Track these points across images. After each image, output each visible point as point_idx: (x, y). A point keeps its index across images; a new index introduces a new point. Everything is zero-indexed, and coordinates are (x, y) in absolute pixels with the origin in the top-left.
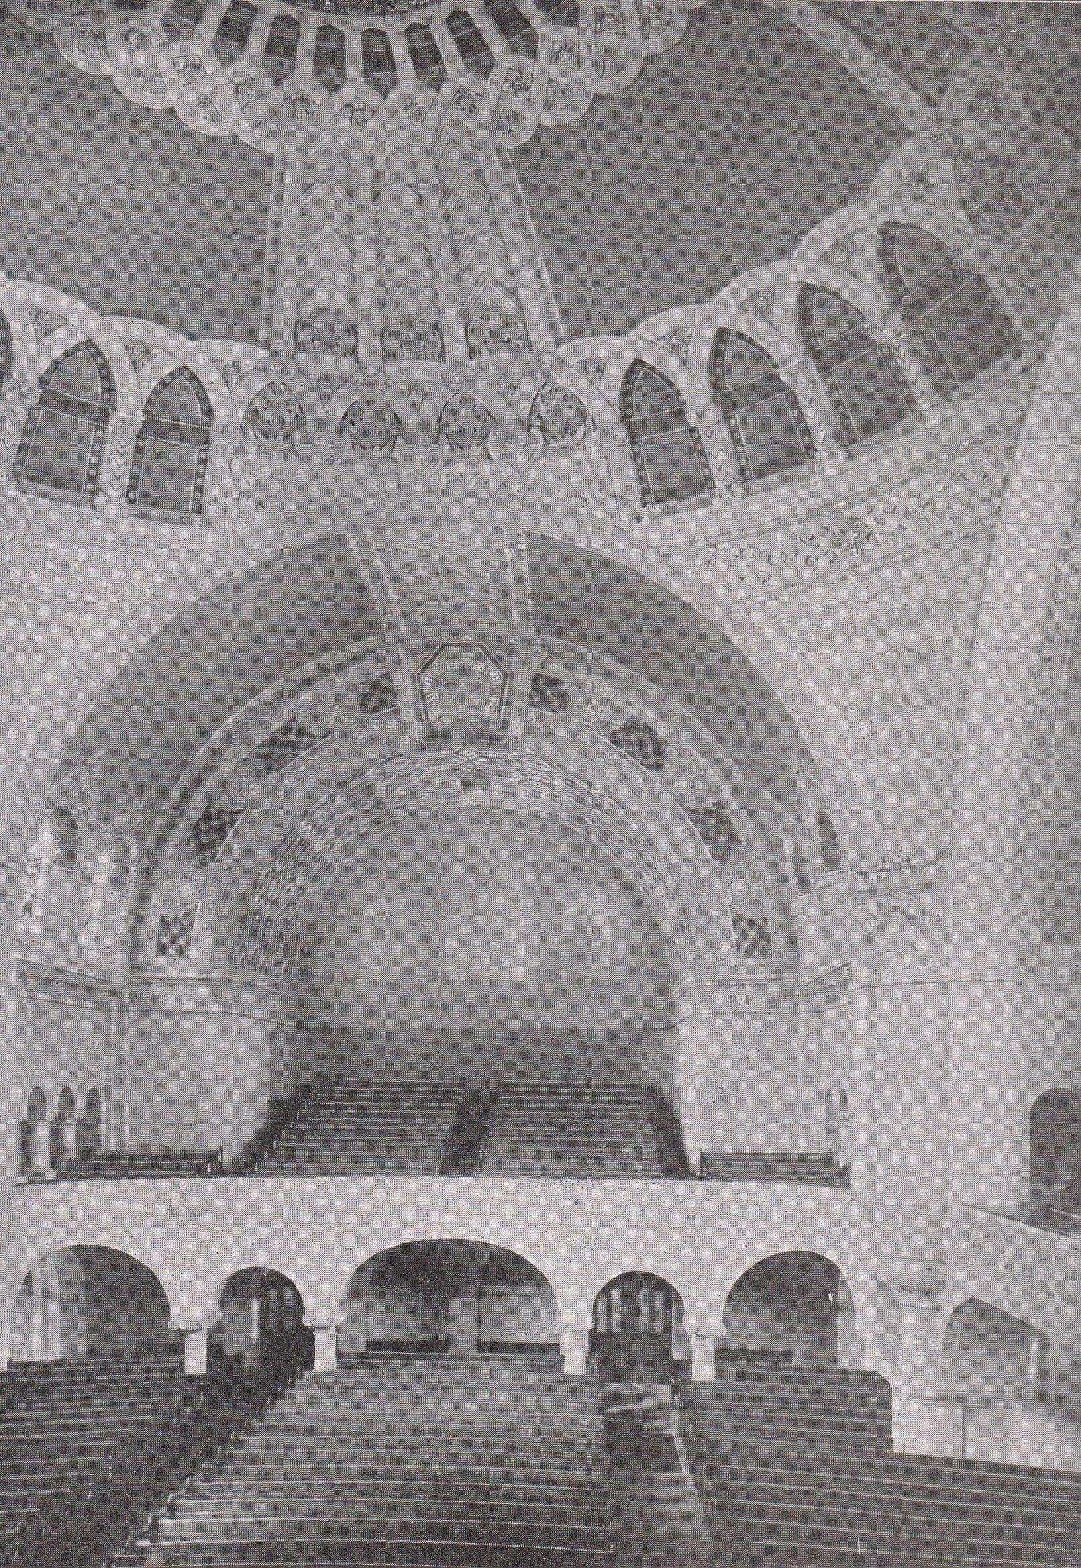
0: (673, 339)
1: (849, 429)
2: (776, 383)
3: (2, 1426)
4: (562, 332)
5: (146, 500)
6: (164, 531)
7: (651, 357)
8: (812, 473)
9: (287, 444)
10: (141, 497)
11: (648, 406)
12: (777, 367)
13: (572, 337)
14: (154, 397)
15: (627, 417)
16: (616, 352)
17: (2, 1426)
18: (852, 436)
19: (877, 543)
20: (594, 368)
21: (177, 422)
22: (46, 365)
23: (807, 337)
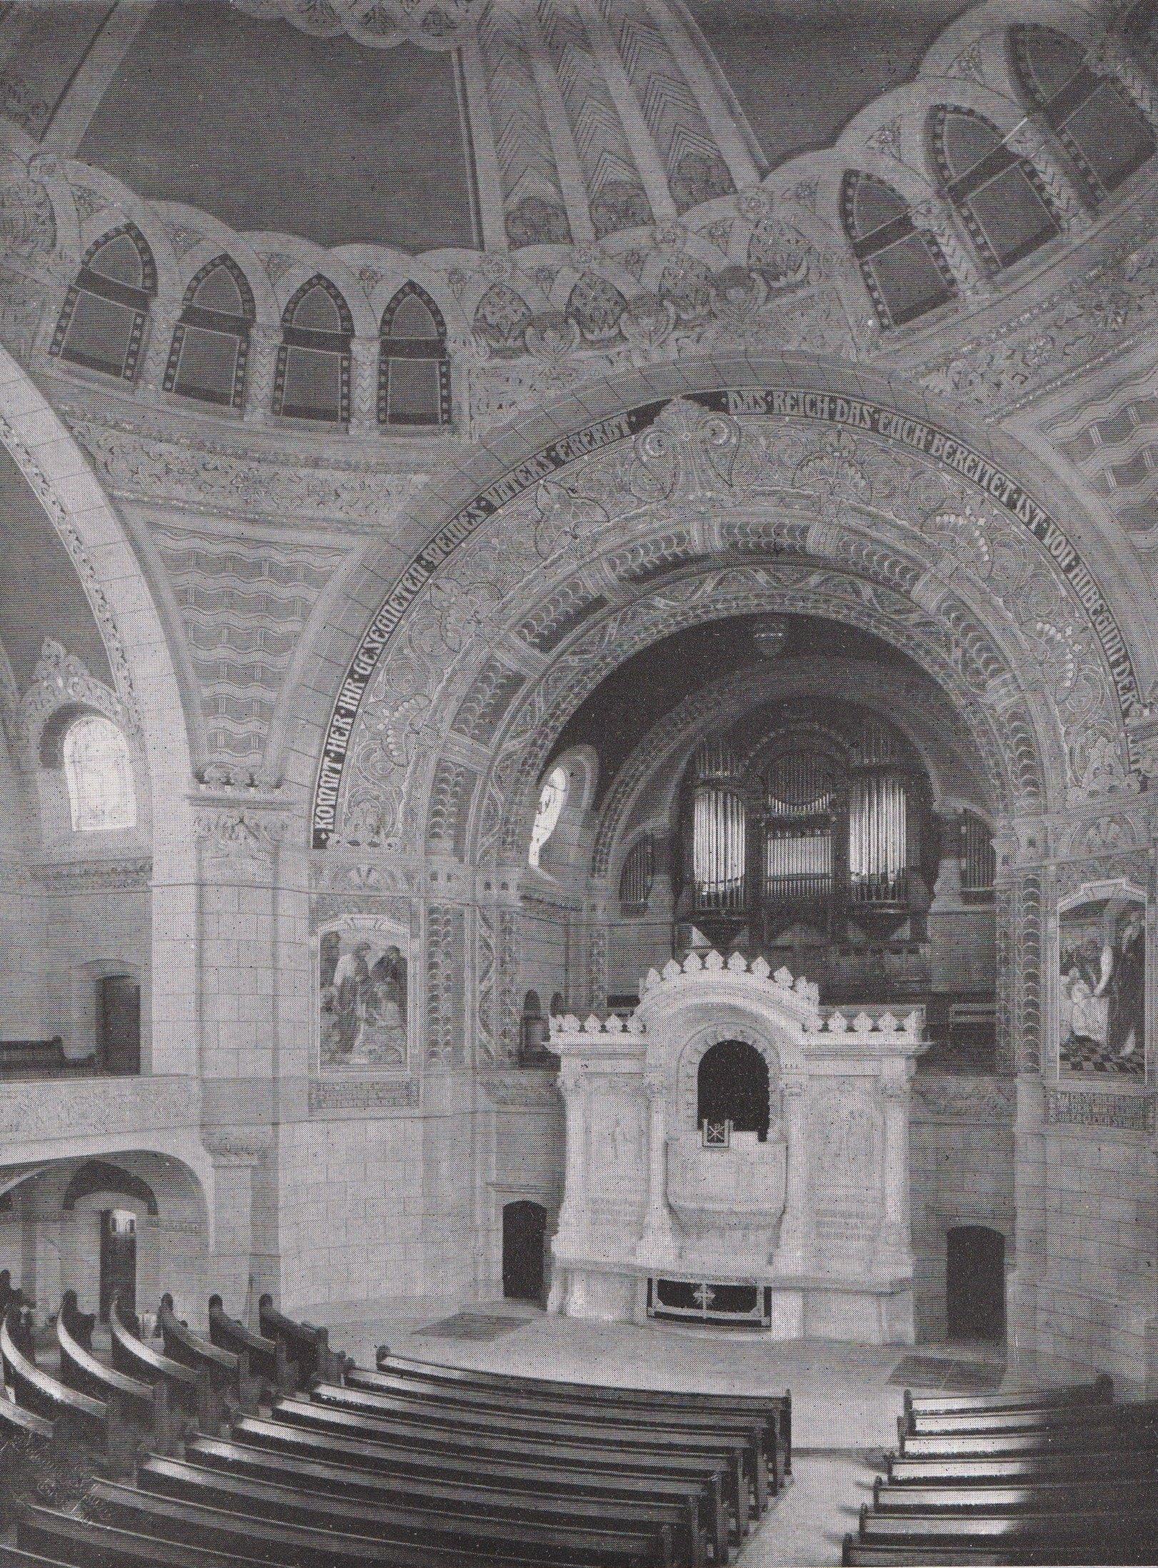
0: (890, 140)
1: (1094, 187)
2: (1003, 157)
3: (5, 1056)
4: (765, 162)
5: (398, 418)
6: (424, 445)
7: (859, 162)
8: (1061, 246)
9: (519, 343)
10: (394, 416)
11: (875, 224)
12: (1003, 136)
13: (775, 164)
14: (388, 317)
15: (852, 238)
16: (822, 168)
17: (5, 1056)
18: (1098, 193)
19: (1140, 308)
20: (806, 192)
21: (415, 342)
22: (89, 245)
23: (1027, 91)
